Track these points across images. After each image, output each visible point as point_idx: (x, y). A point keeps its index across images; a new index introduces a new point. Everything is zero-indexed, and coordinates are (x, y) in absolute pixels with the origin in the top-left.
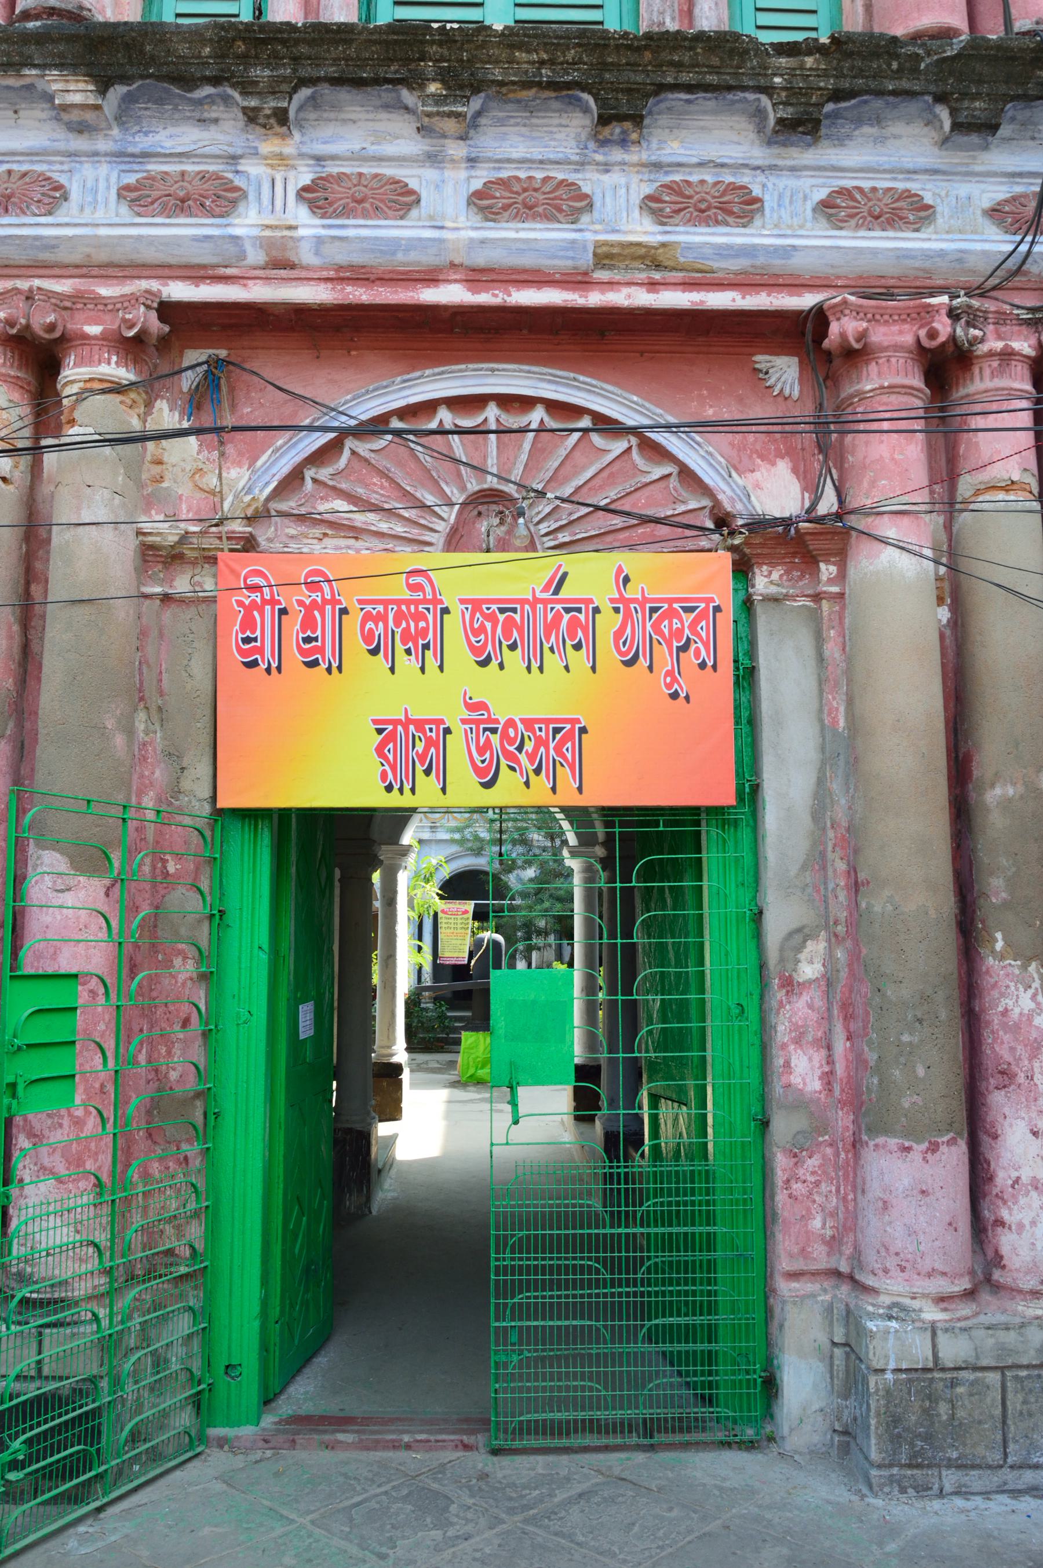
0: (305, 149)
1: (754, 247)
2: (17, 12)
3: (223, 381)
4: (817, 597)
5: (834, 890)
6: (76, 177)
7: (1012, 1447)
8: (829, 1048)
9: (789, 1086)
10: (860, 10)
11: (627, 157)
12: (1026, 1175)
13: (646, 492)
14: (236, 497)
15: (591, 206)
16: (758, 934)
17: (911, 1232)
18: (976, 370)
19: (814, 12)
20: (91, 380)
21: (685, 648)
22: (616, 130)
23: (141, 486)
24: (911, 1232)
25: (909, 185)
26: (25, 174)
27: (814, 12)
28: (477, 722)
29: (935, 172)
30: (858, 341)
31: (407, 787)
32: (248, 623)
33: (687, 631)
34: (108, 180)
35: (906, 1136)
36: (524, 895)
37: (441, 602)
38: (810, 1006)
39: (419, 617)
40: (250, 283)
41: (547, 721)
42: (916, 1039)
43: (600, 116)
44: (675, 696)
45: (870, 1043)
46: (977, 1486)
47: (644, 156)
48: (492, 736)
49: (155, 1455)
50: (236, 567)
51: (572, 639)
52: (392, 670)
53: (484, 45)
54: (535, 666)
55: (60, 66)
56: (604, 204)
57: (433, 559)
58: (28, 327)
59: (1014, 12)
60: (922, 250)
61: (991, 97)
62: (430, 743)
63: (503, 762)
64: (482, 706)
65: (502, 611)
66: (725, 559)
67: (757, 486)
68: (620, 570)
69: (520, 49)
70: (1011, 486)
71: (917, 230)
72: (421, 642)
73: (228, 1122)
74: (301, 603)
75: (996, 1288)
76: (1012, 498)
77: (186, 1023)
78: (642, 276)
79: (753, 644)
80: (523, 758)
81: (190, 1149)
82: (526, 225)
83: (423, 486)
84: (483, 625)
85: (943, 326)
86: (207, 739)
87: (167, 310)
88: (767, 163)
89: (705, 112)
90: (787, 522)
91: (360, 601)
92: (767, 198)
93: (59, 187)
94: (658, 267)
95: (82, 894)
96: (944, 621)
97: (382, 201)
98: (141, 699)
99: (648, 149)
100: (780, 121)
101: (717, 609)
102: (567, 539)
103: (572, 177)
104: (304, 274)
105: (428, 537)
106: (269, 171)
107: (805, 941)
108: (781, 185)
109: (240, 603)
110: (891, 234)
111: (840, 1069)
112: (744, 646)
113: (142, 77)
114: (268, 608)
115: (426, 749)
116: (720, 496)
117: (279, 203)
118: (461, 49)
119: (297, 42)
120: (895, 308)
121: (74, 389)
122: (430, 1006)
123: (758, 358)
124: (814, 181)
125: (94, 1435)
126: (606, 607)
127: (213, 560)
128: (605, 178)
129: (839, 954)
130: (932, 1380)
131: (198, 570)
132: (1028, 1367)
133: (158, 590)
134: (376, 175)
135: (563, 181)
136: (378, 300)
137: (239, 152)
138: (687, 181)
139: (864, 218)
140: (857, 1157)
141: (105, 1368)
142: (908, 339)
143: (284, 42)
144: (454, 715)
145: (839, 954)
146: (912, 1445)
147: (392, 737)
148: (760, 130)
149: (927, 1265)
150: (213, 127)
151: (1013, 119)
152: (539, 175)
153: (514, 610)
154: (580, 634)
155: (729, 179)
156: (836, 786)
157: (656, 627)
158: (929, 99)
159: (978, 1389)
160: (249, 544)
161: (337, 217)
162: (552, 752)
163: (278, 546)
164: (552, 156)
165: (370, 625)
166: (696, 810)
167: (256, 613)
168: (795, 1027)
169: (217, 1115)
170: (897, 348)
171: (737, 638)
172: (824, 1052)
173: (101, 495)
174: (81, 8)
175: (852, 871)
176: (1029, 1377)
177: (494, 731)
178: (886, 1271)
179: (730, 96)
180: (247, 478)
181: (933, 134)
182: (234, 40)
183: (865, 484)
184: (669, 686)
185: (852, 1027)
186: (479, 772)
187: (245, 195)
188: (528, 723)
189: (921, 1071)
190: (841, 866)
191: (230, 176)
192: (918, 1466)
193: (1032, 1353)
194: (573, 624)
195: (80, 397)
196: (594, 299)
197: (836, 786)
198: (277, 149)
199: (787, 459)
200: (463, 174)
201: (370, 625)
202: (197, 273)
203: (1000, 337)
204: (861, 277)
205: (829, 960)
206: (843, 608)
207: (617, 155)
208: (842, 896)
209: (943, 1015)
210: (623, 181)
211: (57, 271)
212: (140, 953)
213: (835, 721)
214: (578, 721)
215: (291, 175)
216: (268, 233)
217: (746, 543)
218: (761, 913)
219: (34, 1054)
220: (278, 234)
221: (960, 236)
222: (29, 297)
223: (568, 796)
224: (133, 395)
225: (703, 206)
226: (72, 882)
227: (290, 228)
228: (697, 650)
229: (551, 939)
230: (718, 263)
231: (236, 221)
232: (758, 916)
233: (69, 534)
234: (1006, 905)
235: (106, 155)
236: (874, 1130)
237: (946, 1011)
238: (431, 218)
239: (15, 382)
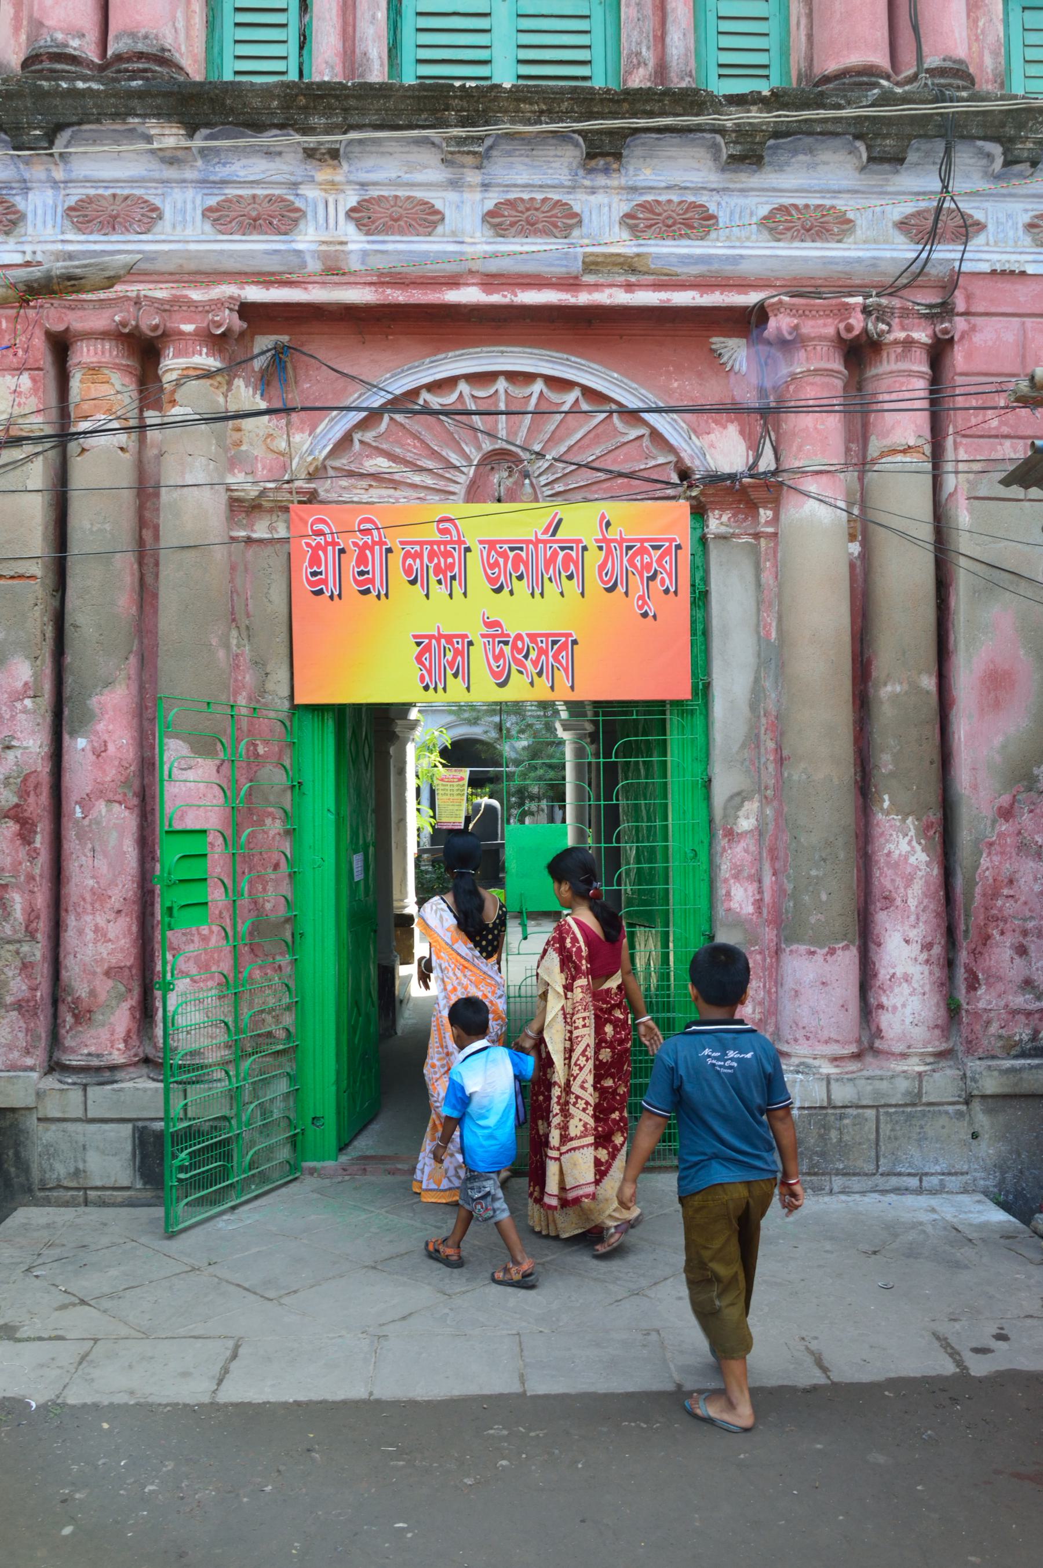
0: (352, 178)
1: (710, 256)
2: (110, 53)
3: (289, 365)
4: (757, 536)
5: (765, 763)
6: (168, 200)
7: (882, 1161)
8: (760, 881)
9: (729, 910)
10: (803, 39)
11: (609, 182)
12: (899, 971)
13: (625, 449)
14: (301, 458)
15: (580, 223)
16: (708, 798)
17: (814, 1012)
18: (884, 354)
19: (767, 35)
20: (187, 368)
21: (653, 578)
22: (601, 162)
23: (226, 450)
24: (814, 1012)
25: (835, 202)
26: (126, 198)
27: (767, 35)
28: (494, 636)
29: (856, 192)
30: (790, 334)
31: (440, 687)
32: (315, 560)
33: (655, 565)
34: (194, 202)
35: (812, 944)
36: (517, 763)
37: (464, 542)
38: (746, 851)
39: (447, 554)
40: (310, 286)
41: (547, 636)
42: (821, 874)
43: (588, 154)
44: (645, 615)
45: (788, 877)
46: (856, 1187)
47: (623, 181)
48: (505, 648)
49: (263, 1178)
50: (303, 515)
51: (566, 571)
52: (427, 596)
53: (496, 99)
54: (537, 592)
55: (158, 116)
56: (590, 221)
57: (456, 509)
58: (137, 327)
59: (925, 49)
60: (844, 257)
61: (900, 137)
62: (457, 653)
63: (514, 667)
64: (497, 624)
65: (512, 549)
66: (683, 507)
67: (712, 446)
68: (603, 516)
69: (524, 102)
70: (907, 450)
71: (839, 241)
72: (449, 574)
73: (309, 940)
74: (355, 544)
75: (876, 1052)
76: (908, 459)
77: (276, 867)
78: (621, 279)
79: (707, 571)
80: (528, 664)
81: (284, 960)
82: (529, 240)
83: (448, 445)
84: (497, 561)
85: (857, 321)
86: (286, 651)
87: (247, 310)
88: (721, 186)
89: (672, 146)
90: (732, 477)
91: (402, 543)
92: (721, 214)
93: (155, 209)
94: (634, 271)
95: (200, 771)
96: (856, 554)
97: (414, 219)
98: (234, 620)
99: (626, 175)
100: (731, 156)
101: (678, 547)
102: (561, 489)
103: (565, 198)
104: (352, 279)
105: (452, 488)
106: (323, 194)
107: (743, 802)
108: (733, 204)
109: (308, 545)
110: (818, 244)
111: (767, 897)
112: (699, 575)
113: (223, 124)
114: (330, 548)
115: (454, 658)
116: (683, 454)
117: (331, 221)
118: (477, 102)
119: (347, 97)
120: (821, 305)
121: (174, 376)
122: (430, 868)
123: (714, 340)
124: (758, 200)
125: (228, 1156)
126: (592, 546)
127: (286, 509)
128: (592, 198)
129: (768, 811)
130: (826, 1115)
131: (274, 518)
132: (896, 1106)
133: (243, 534)
134: (409, 198)
135: (559, 201)
136: (412, 301)
137: (300, 179)
138: (657, 201)
139: (798, 231)
140: (778, 960)
141: (234, 1112)
142: (831, 331)
143: (336, 97)
144: (475, 631)
145: (768, 811)
146: (811, 1159)
147: (428, 648)
148: (716, 158)
149: (825, 1034)
150: (278, 159)
151: (918, 150)
152: (539, 196)
153: (521, 549)
154: (572, 567)
155: (691, 198)
156: (768, 684)
157: (631, 561)
158: (850, 138)
159: (859, 1121)
160: (312, 498)
161: (379, 233)
162: (551, 659)
163: (333, 496)
164: (549, 182)
165: (410, 561)
166: (663, 703)
167: (321, 553)
168: (735, 866)
169: (302, 935)
170: (821, 338)
171: (694, 568)
172: (756, 885)
173: (200, 462)
174: (163, 50)
175: (779, 749)
176: (896, 1112)
177: (506, 643)
178: (796, 1040)
179: (692, 135)
180: (310, 442)
181: (855, 161)
182: (297, 95)
183: (794, 448)
184: (640, 608)
185: (777, 866)
186: (495, 675)
187: (304, 214)
188: (533, 637)
189: (824, 897)
190: (771, 745)
191: (291, 198)
192: (815, 1174)
193: (899, 1096)
194: (567, 559)
195: (178, 384)
196: (583, 298)
197: (768, 684)
198: (329, 177)
199: (736, 423)
200: (478, 196)
201: (410, 561)
202: (267, 279)
203: (903, 328)
204: (795, 279)
205: (761, 817)
206: (776, 545)
207: (601, 180)
208: (771, 767)
209: (842, 855)
210: (606, 201)
211: (155, 278)
212: (243, 814)
213: (768, 634)
214: (571, 635)
215: (341, 197)
216: (324, 248)
217: (702, 493)
218: (710, 780)
219: (183, 886)
220: (332, 248)
221: (874, 246)
222: (137, 302)
223: (563, 693)
224: (219, 378)
225: (670, 222)
226: (192, 762)
227: (342, 243)
228: (663, 579)
229: (544, 804)
230: (678, 270)
231: (299, 238)
232: (708, 783)
233: (176, 494)
234: (892, 775)
235: (192, 182)
236: (789, 940)
237: (844, 853)
238: (454, 233)
239: (126, 370)
